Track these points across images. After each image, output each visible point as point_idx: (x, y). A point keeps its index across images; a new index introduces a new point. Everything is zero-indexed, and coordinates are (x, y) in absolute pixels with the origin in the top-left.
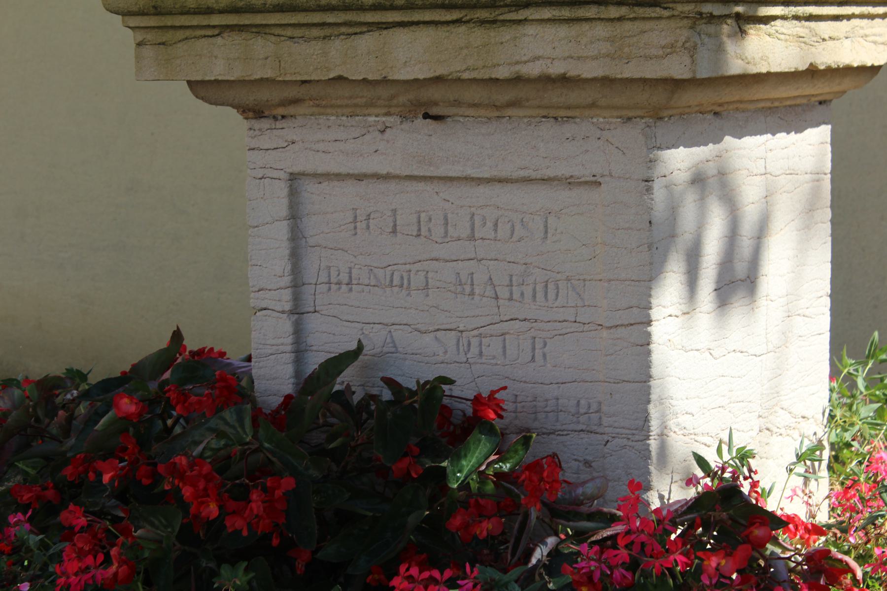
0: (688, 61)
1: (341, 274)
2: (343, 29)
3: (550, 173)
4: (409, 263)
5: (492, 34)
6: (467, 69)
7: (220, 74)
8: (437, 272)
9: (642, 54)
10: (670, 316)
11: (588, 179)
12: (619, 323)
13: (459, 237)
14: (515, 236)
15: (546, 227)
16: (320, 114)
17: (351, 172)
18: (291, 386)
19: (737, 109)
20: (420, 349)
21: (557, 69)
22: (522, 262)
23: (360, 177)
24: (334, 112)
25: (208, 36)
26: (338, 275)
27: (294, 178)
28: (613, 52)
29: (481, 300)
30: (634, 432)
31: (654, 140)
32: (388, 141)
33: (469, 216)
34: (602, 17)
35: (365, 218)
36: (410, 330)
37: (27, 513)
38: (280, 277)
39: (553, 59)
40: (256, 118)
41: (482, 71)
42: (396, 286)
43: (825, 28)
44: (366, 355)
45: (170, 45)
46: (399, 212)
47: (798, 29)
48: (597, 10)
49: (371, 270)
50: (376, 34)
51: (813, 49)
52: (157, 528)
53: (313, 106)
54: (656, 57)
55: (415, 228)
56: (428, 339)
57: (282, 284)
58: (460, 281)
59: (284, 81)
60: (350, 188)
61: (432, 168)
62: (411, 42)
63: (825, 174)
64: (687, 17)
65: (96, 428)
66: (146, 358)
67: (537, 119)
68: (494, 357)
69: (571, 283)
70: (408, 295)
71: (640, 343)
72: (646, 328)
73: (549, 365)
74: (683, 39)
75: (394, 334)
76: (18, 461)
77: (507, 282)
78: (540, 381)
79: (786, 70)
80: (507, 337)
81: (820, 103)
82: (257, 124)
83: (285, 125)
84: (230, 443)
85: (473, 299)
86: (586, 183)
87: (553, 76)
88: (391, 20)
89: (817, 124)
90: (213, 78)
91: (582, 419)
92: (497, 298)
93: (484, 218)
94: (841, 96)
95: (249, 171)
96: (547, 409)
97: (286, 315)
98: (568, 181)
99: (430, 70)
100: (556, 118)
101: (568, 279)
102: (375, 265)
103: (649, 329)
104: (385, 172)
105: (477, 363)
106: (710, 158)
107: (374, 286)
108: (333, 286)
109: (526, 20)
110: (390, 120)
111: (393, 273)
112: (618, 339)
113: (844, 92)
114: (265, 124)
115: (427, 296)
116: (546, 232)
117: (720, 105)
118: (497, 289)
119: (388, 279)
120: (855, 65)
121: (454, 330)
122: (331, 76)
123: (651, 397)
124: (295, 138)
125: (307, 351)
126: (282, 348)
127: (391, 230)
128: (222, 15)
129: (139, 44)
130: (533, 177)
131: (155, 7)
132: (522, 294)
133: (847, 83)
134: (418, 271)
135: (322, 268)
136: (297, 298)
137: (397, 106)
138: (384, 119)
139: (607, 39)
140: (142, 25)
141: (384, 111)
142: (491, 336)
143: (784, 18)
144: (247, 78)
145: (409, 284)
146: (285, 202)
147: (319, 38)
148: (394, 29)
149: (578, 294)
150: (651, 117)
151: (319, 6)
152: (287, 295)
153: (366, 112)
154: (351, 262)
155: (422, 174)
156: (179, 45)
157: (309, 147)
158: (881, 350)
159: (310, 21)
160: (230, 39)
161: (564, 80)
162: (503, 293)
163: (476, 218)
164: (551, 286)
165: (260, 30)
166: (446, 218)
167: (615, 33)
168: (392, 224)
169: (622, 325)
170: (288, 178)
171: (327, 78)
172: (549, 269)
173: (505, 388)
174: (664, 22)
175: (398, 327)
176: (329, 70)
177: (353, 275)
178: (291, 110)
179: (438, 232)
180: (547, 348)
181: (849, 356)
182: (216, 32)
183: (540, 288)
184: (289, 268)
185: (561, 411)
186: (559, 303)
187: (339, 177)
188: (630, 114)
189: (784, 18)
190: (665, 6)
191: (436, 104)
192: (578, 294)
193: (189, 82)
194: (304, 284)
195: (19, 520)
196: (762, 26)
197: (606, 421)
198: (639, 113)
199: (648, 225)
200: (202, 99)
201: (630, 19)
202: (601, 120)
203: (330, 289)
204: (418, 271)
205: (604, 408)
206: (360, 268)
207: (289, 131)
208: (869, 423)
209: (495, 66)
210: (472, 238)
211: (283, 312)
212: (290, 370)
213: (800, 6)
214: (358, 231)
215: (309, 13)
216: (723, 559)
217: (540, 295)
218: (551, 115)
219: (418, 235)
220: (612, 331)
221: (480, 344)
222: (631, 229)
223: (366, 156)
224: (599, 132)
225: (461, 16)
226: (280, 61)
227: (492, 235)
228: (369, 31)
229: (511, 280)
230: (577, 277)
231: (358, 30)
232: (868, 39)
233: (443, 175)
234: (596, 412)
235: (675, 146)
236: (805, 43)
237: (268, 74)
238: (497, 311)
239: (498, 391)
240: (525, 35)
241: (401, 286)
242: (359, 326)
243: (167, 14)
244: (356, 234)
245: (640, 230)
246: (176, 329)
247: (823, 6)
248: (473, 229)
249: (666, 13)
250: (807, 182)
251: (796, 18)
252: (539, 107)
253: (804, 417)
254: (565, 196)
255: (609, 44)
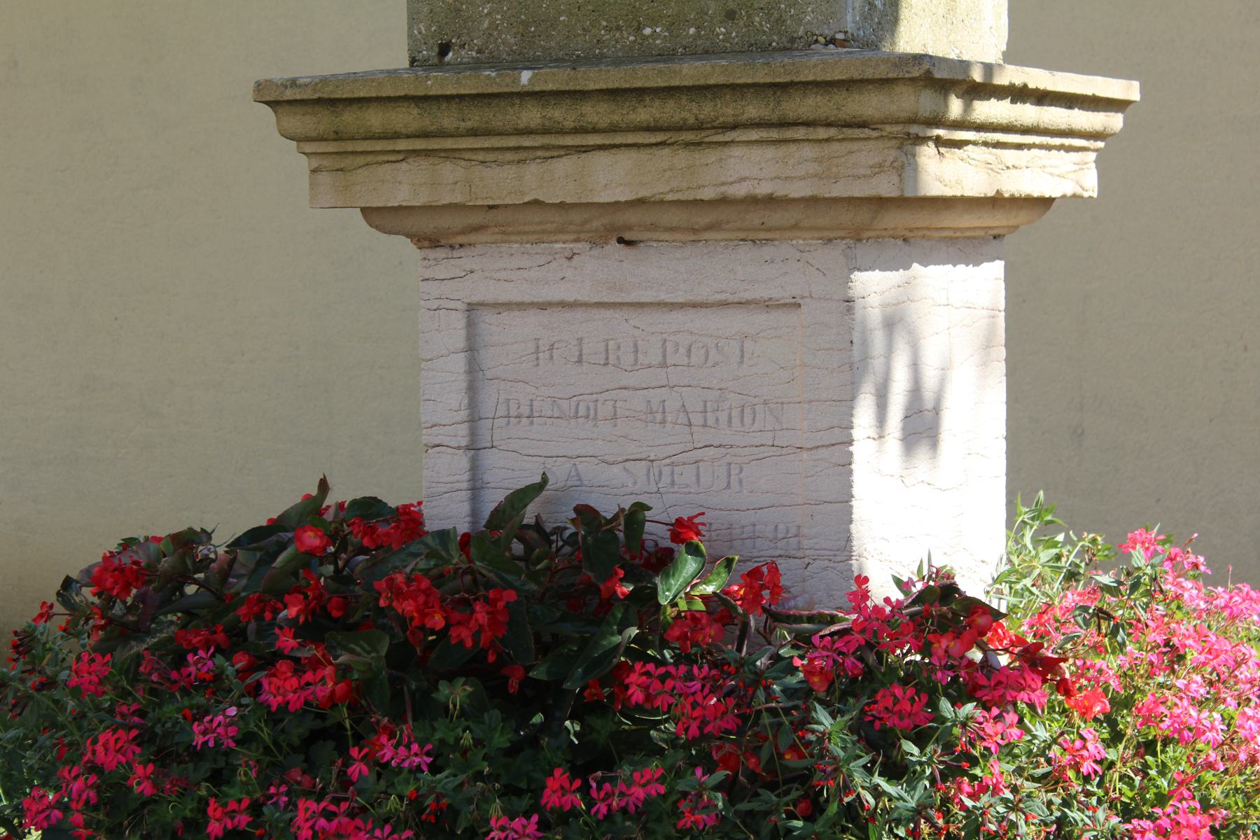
0: (895, 179)
1: (522, 407)
2: (539, 153)
3: (748, 296)
4: (597, 393)
5: (697, 156)
6: (671, 191)
7: (405, 200)
8: (626, 401)
9: (850, 173)
10: (869, 438)
11: (787, 301)
12: (821, 443)
13: (650, 364)
14: (709, 361)
15: (742, 351)
16: (503, 242)
17: (535, 300)
18: (467, 525)
19: (924, 236)
20: (608, 480)
21: (763, 189)
22: (717, 387)
23: (543, 306)
24: (519, 239)
25: (391, 162)
26: (519, 408)
27: (472, 308)
28: (821, 171)
29: (674, 427)
30: (836, 552)
31: (854, 261)
32: (576, 268)
33: (661, 343)
34: (811, 138)
35: (548, 348)
36: (596, 461)
37: (209, 650)
38: (456, 411)
39: (760, 180)
40: (431, 247)
41: (687, 193)
42: (581, 417)
43: (1009, 156)
44: (548, 490)
45: (349, 171)
46: (586, 341)
47: (986, 155)
48: (805, 131)
49: (555, 401)
50: (575, 157)
51: (999, 176)
52: (359, 655)
53: (498, 233)
54: (864, 176)
55: (603, 356)
56: (616, 469)
57: (458, 419)
58: (651, 408)
59: (475, 206)
60: (532, 317)
61: (623, 295)
62: (611, 166)
63: (1000, 311)
64: (895, 138)
65: (274, 565)
66: (292, 507)
67: (735, 243)
68: (687, 486)
69: (769, 407)
70: (594, 426)
71: (842, 463)
72: (848, 447)
73: (745, 491)
74: (891, 159)
75: (579, 467)
76: (160, 615)
77: (700, 408)
78: (736, 508)
79: (977, 195)
80: (701, 464)
81: (995, 238)
82: (432, 254)
83: (462, 254)
84: (441, 562)
85: (664, 427)
86: (785, 305)
87: (760, 197)
88: (591, 143)
89: (992, 259)
90: (396, 205)
91: (779, 544)
92: (690, 425)
93: (677, 345)
94: (1014, 232)
95: (422, 302)
96: (742, 536)
97: (462, 451)
98: (767, 303)
99: (632, 192)
100: (754, 241)
101: (765, 403)
102: (558, 396)
103: (851, 448)
104: (572, 300)
105: (670, 492)
106: (901, 284)
107: (558, 418)
108: (512, 420)
109: (732, 142)
110: (578, 247)
111: (578, 404)
112: (819, 460)
113: (1017, 227)
114: (440, 253)
115: (615, 426)
116: (742, 356)
117: (911, 230)
118: (691, 416)
119: (573, 411)
120: (1035, 196)
121: (645, 459)
122: (526, 200)
123: (853, 516)
124: (474, 267)
125: (483, 488)
126: (457, 486)
127: (576, 360)
128: (408, 140)
129: (314, 171)
130: (730, 301)
131: (336, 133)
132: (717, 420)
133: (1021, 217)
134: (605, 401)
135: (500, 401)
136: (473, 434)
137: (588, 232)
138: (571, 246)
139: (815, 160)
140: (320, 151)
141: (573, 237)
142: (684, 464)
143: (975, 143)
144: (434, 204)
145: (596, 414)
146: (463, 333)
147: (513, 161)
148: (594, 152)
149: (775, 417)
150: (851, 238)
151: (516, 130)
152: (463, 430)
153: (554, 238)
154: (533, 394)
155: (612, 301)
156: (359, 171)
157: (489, 275)
158: (1046, 510)
159: (505, 145)
160: (416, 164)
161: (771, 201)
162: (697, 419)
163: (668, 344)
164: (747, 411)
165: (449, 154)
166: (636, 346)
167: (823, 154)
168: (577, 353)
169: (823, 446)
170: (466, 308)
171: (521, 202)
172: (745, 393)
173: (703, 514)
174: (872, 142)
175: (583, 459)
176: (523, 193)
177: (534, 408)
178: (472, 238)
179: (627, 359)
180: (743, 474)
181: (1023, 505)
182: (401, 157)
183: (735, 413)
184: (466, 402)
185: (758, 537)
186: (756, 427)
187: (521, 306)
188: (832, 235)
189: (975, 143)
190: (874, 127)
191: (630, 228)
192: (775, 417)
193: (365, 211)
194: (480, 419)
195: (201, 657)
196: (956, 150)
197: (806, 543)
198: (842, 234)
199: (850, 344)
200: (377, 227)
201: (839, 140)
202: (801, 242)
203: (508, 423)
204: (605, 401)
205: (804, 531)
206: (543, 400)
207: (467, 259)
208: (1050, 567)
209: (699, 188)
210: (663, 365)
211: (459, 448)
212: (466, 508)
213: (989, 132)
214: (541, 362)
215: (503, 137)
216: (951, 641)
217: (736, 421)
218: (750, 238)
219: (606, 364)
220: (812, 452)
221: (672, 473)
222: (832, 349)
223: (552, 283)
224: (799, 254)
225: (666, 138)
226: (470, 186)
227: (686, 361)
228: (566, 155)
229: (705, 407)
230: (775, 401)
231: (555, 154)
232: (1045, 170)
233: (635, 301)
234: (796, 536)
235: (870, 268)
236: (992, 169)
237: (458, 198)
238: (690, 438)
239: (696, 516)
240: (731, 156)
241: (587, 417)
242: (542, 459)
243: (349, 139)
244: (538, 365)
245: (840, 350)
246: (322, 477)
247: (1008, 133)
248: (664, 356)
249: (875, 134)
250: (984, 318)
251: (986, 144)
252: (739, 229)
253: (983, 562)
254: (762, 319)
255: (816, 164)
